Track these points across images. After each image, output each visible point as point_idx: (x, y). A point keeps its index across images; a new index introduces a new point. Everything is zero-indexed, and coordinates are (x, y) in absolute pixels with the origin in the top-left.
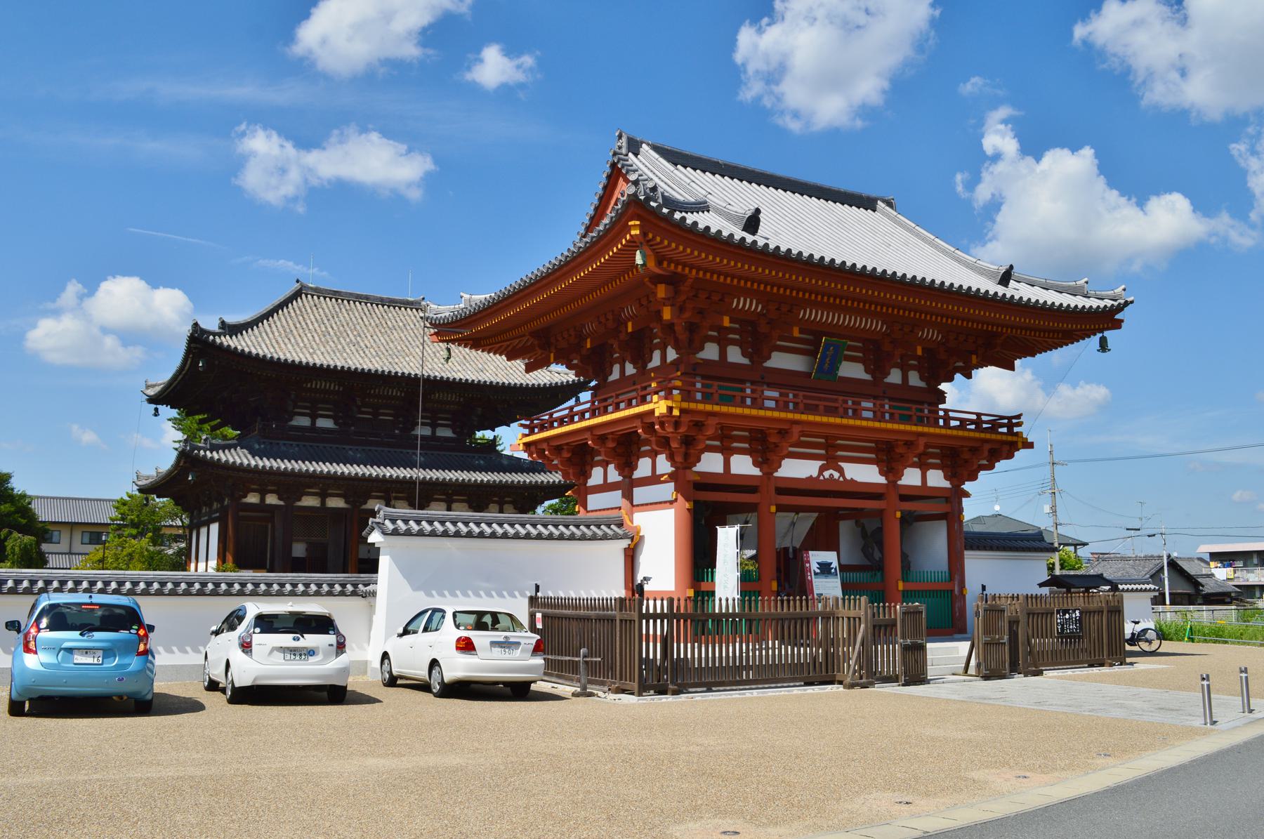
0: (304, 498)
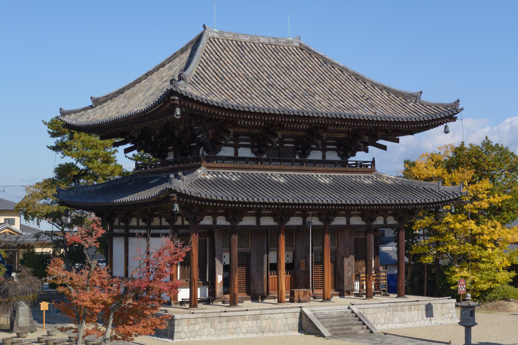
0: (244, 219)
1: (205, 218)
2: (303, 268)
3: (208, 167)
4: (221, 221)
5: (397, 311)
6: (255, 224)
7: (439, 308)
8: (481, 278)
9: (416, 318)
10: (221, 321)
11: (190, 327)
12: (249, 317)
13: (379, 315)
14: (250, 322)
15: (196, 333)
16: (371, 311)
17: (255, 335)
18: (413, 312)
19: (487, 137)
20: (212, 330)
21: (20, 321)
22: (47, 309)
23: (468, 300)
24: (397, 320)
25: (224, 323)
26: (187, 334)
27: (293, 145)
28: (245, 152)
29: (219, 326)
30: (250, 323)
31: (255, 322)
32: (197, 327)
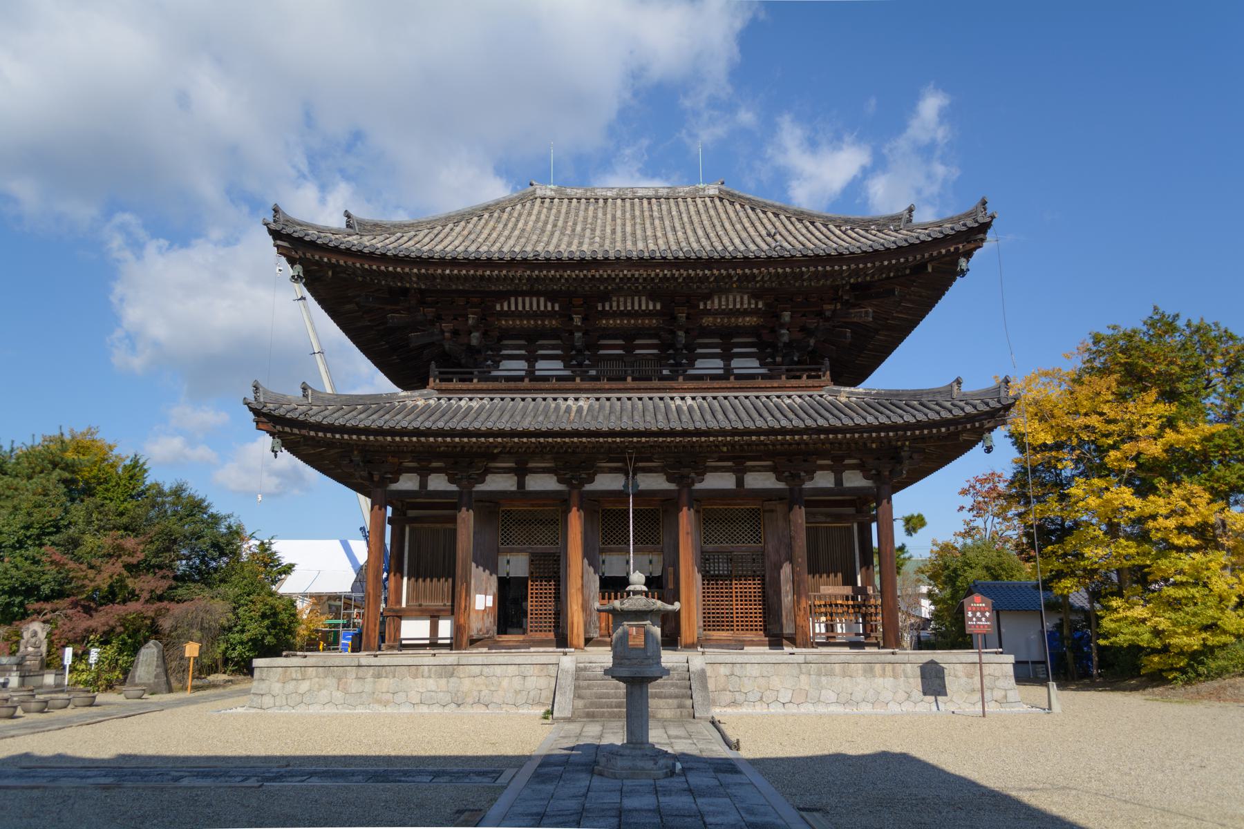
0: (489, 478)
1: (401, 478)
2: (671, 586)
3: (440, 391)
4: (439, 483)
5: (831, 674)
6: (514, 488)
7: (960, 674)
8: (1176, 623)
9: (887, 695)
10: (361, 674)
11: (287, 685)
12: (430, 671)
13: (776, 682)
14: (431, 681)
15: (298, 699)
16: (754, 671)
17: (436, 710)
18: (880, 681)
19: (1155, 309)
20: (338, 695)
21: (137, 674)
22: (196, 654)
23: (635, 593)
24: (830, 695)
25: (370, 680)
26: (278, 699)
27: (655, 351)
28: (549, 367)
29: (354, 686)
30: (431, 683)
31: (443, 681)
32: (304, 686)
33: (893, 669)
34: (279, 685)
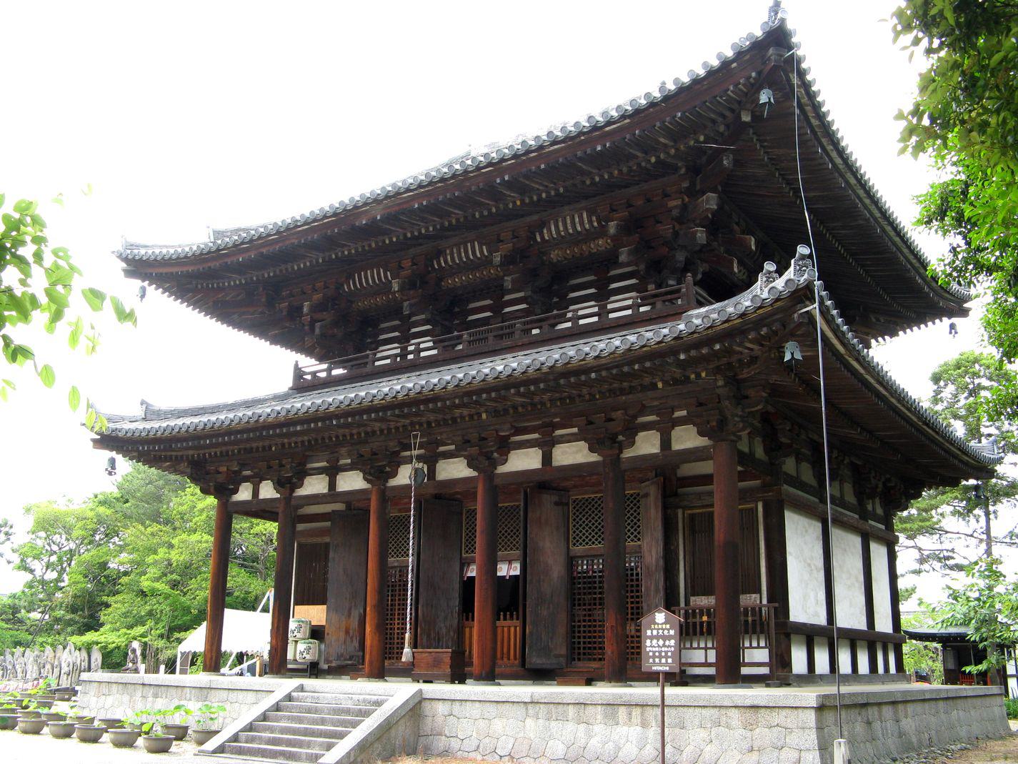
6: (326, 491)
25: (150, 699)
33: (642, 714)
34: (95, 699)
